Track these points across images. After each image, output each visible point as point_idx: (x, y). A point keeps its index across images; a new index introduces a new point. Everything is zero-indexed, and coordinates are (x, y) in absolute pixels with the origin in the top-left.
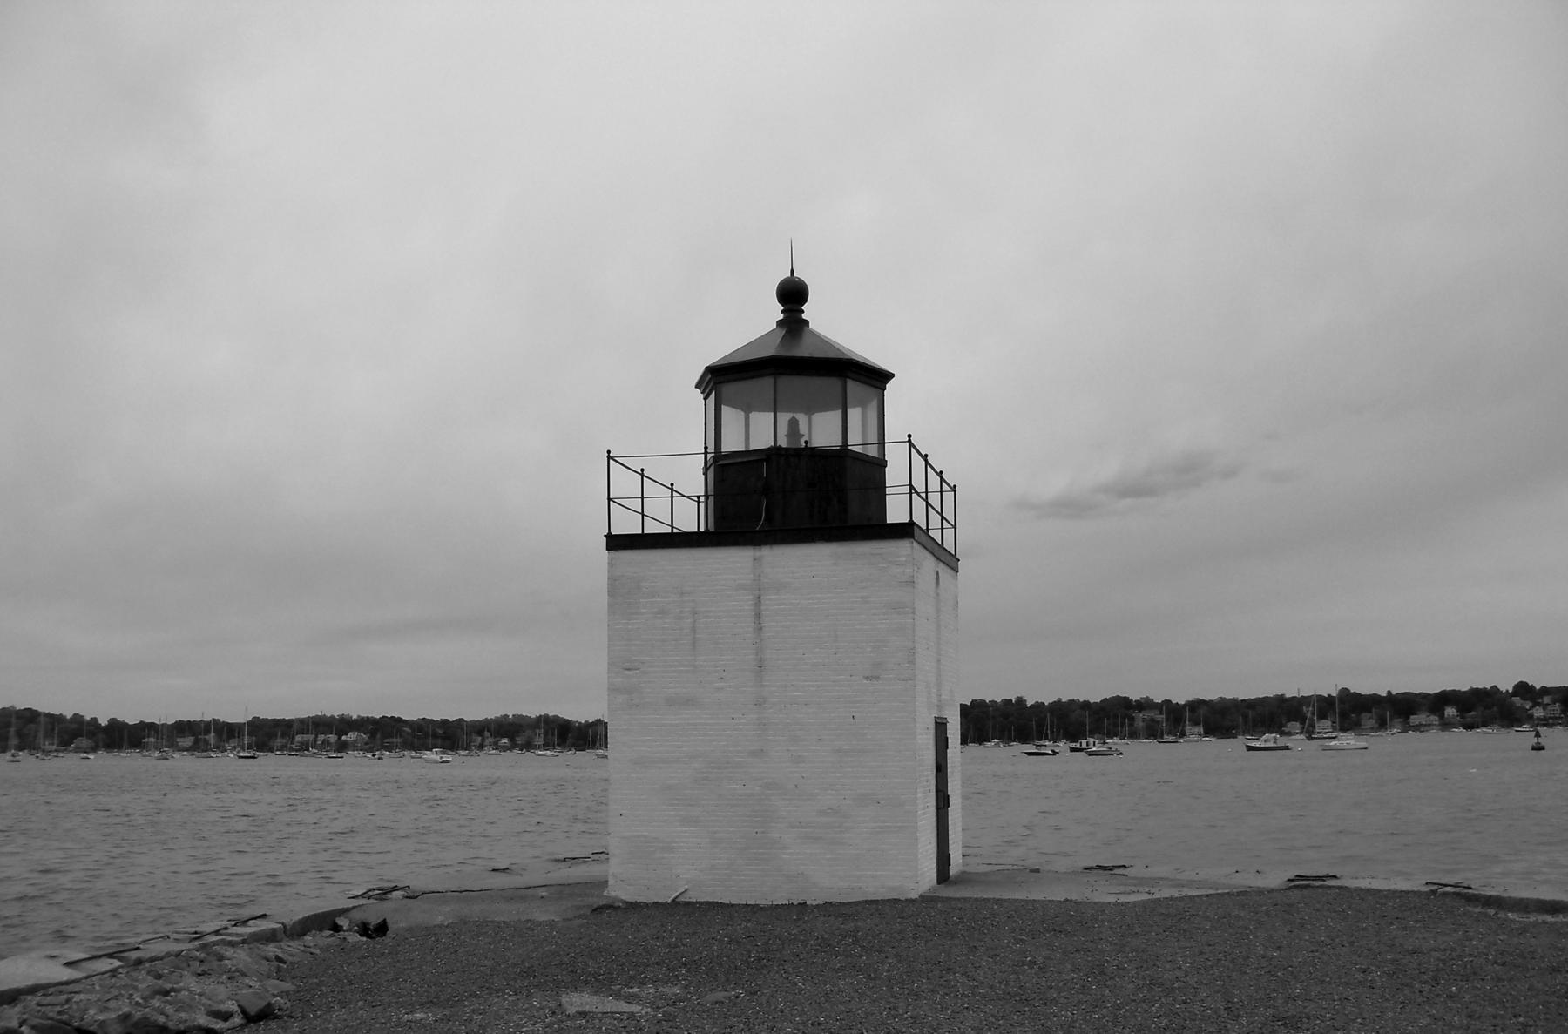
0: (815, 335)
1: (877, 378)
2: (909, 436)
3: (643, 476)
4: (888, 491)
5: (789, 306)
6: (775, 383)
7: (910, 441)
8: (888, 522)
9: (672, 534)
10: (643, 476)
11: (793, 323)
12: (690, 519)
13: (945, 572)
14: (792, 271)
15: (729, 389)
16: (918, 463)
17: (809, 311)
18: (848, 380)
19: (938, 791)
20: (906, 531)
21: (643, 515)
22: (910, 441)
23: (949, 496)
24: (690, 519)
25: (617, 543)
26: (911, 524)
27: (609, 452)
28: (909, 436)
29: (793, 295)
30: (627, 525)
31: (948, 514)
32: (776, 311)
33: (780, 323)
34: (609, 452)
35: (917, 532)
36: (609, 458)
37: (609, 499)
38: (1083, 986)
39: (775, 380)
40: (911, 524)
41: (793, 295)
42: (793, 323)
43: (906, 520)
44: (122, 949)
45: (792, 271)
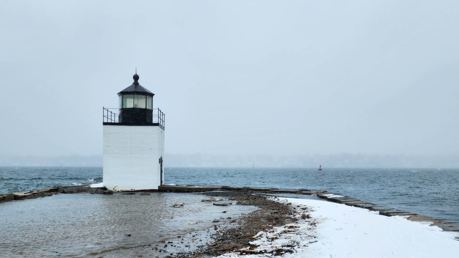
0: (140, 86)
1: (152, 95)
2: (158, 108)
3: (111, 113)
4: (153, 116)
5: (136, 80)
6: (134, 96)
7: (158, 109)
8: (153, 123)
9: (115, 123)
10: (111, 113)
11: (136, 83)
12: (117, 121)
13: (163, 130)
14: (136, 73)
15: (125, 96)
16: (159, 112)
17: (139, 81)
18: (147, 96)
19: (161, 169)
20: (157, 124)
21: (108, 118)
22: (158, 109)
23: (163, 116)
24: (117, 121)
25: (105, 124)
26: (158, 123)
27: (103, 107)
28: (158, 108)
29: (136, 78)
30: (106, 121)
31: (163, 120)
32: (133, 81)
33: (133, 83)
34: (103, 107)
35: (159, 125)
36: (103, 108)
37: (104, 116)
38: (78, 229)
39: (138, 101)
40: (158, 123)
41: (136, 78)
42: (136, 83)
43: (157, 123)
44: (399, 212)
45: (136, 73)
